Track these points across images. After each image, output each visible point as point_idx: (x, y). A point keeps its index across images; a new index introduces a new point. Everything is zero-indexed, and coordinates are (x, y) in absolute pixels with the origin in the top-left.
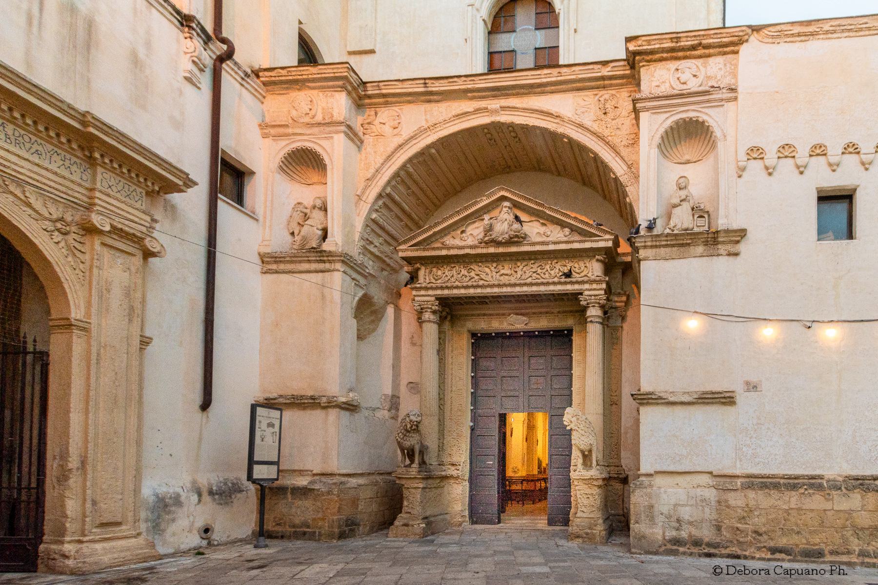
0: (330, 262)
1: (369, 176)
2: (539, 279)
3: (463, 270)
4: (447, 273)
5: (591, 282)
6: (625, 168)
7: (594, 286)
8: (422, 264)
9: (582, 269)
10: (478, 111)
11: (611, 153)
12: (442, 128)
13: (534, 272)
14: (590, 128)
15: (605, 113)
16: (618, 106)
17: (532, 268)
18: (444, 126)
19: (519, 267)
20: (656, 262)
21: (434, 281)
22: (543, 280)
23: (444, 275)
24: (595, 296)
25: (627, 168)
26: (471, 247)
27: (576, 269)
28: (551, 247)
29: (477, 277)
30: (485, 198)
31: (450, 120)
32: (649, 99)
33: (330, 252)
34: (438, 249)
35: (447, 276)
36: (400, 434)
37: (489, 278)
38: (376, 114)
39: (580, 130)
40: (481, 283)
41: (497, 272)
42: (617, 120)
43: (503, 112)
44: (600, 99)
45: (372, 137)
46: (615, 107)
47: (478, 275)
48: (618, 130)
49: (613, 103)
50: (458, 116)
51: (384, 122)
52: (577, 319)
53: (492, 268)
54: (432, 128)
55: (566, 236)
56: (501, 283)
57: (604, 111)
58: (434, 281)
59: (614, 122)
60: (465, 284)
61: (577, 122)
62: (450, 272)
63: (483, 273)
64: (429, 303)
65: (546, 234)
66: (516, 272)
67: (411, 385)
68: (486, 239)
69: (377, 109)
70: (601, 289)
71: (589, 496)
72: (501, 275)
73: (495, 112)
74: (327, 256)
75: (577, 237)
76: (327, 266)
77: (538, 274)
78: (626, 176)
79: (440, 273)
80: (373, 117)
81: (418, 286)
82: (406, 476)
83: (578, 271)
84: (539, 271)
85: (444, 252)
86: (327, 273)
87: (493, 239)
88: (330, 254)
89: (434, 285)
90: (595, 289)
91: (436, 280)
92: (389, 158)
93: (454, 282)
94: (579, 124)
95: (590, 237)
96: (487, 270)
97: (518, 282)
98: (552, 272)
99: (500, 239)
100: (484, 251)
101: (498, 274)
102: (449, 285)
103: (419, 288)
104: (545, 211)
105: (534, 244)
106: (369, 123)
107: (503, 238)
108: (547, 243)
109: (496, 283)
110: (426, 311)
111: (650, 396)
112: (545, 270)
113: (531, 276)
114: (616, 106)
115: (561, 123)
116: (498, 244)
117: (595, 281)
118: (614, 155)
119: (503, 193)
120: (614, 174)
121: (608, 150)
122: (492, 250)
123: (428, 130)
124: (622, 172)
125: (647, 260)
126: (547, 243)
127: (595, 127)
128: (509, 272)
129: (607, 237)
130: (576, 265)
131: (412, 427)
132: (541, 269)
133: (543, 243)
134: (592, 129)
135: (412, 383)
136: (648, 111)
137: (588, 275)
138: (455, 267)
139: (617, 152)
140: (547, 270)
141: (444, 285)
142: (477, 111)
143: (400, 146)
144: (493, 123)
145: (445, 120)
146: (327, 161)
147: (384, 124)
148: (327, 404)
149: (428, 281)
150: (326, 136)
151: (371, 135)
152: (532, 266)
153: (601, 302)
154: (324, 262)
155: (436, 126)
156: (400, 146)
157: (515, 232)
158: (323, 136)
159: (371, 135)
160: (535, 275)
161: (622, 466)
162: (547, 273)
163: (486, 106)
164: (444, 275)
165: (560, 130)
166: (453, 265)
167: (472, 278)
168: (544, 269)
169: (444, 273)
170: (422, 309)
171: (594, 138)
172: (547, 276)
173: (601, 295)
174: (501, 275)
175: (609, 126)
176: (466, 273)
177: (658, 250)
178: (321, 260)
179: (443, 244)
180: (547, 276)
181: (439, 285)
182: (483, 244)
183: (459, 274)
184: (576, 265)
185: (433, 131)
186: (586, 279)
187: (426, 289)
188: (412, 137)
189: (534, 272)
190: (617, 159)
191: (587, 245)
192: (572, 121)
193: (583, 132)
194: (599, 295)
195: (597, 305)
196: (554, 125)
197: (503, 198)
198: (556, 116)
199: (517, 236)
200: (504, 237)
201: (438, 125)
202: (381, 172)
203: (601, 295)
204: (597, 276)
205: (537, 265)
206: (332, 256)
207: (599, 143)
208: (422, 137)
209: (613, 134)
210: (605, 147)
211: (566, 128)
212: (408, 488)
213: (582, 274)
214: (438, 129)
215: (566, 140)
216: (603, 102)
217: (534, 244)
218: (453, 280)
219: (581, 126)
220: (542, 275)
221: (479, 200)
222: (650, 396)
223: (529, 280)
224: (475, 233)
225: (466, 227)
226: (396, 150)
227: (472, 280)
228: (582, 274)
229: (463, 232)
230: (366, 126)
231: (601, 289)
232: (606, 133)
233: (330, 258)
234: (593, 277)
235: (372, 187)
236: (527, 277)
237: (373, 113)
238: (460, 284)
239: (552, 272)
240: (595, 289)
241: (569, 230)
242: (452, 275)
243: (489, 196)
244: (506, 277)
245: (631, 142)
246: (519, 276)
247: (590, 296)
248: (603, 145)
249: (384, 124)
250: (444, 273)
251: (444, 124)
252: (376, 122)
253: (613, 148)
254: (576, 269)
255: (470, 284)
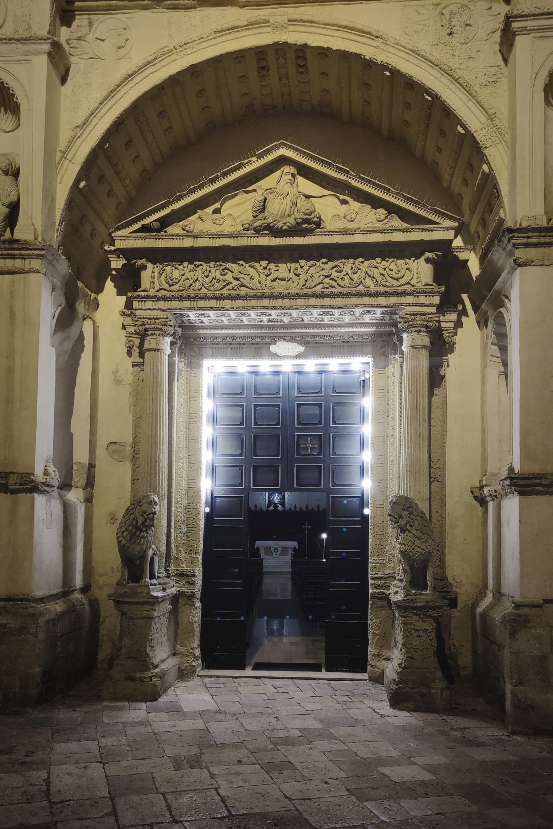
0: (23, 257)
1: (80, 121)
2: (334, 287)
3: (213, 270)
4: (187, 275)
5: (415, 293)
6: (484, 119)
7: (422, 299)
8: (149, 260)
9: (403, 272)
10: (252, 25)
11: (460, 95)
12: (194, 50)
13: (327, 277)
14: (430, 57)
15: (450, 34)
16: (471, 22)
17: (323, 269)
18: (199, 47)
19: (302, 267)
20: (544, 268)
21: (166, 286)
22: (342, 289)
23: (184, 278)
24: (421, 315)
25: (485, 119)
26: (231, 236)
27: (393, 273)
28: (358, 239)
29: (235, 283)
30: (254, 159)
31: (209, 38)
32: (534, 15)
33: (26, 242)
34: (178, 236)
35: (188, 279)
36: (126, 533)
37: (255, 284)
38: (90, 24)
39: (412, 59)
40: (243, 291)
41: (267, 276)
42: (470, 44)
43: (290, 28)
44: (444, 11)
45: (83, 61)
46: (467, 25)
47: (237, 279)
48: (471, 60)
49: (464, 18)
50: (222, 32)
51: (103, 38)
52: (378, 348)
53: (260, 269)
54: (180, 49)
55: (379, 221)
56: (276, 292)
57: (449, 31)
58: (166, 286)
59: (465, 46)
60: (218, 293)
61: (408, 46)
62: (192, 273)
63: (245, 277)
64: (158, 321)
65: (348, 218)
66: (298, 275)
67: (113, 447)
68: (257, 224)
69: (92, 16)
70: (431, 305)
71: (421, 633)
72: (274, 280)
73: (281, 27)
74: (20, 249)
75: (396, 222)
76: (18, 263)
77: (333, 279)
78: (484, 132)
79: (176, 274)
80: (85, 30)
81: (143, 294)
82: (132, 600)
83: (396, 276)
84: (334, 274)
85: (187, 243)
86: (18, 275)
87: (269, 224)
88: (25, 245)
89: (168, 294)
90: (422, 305)
91: (171, 285)
92: (112, 93)
93: (200, 290)
94: (411, 50)
95: (418, 224)
96: (252, 271)
97: (303, 292)
98: (355, 277)
99: (280, 225)
100: (252, 242)
101: (269, 278)
102: (193, 293)
103: (144, 297)
104: (350, 181)
105: (331, 233)
106: (79, 39)
107: (285, 224)
108: (352, 233)
109: (267, 291)
110: (152, 334)
111: (537, 481)
112: (344, 273)
113: (321, 283)
114: (468, 22)
115: (383, 46)
116: (275, 232)
117: (423, 293)
118: (465, 99)
119: (283, 151)
120: (464, 127)
121: (456, 91)
122: (265, 241)
123: (174, 51)
124: (479, 126)
125: (530, 265)
126: (352, 233)
127: (435, 54)
128: (286, 275)
129: (448, 223)
130: (393, 266)
131: (145, 521)
132: (336, 271)
133: (345, 232)
134: (433, 59)
135: (115, 443)
136: (529, 34)
137: (412, 282)
138: (201, 265)
139: (471, 95)
140: (347, 274)
141: (184, 294)
142: (252, 25)
143: (130, 76)
144: (276, 44)
145: (202, 38)
146: (20, 98)
147: (103, 40)
148: (18, 487)
149: (157, 286)
150: (20, 58)
151: (82, 57)
152: (323, 266)
153: (431, 324)
154: (13, 257)
155: (185, 47)
156: (130, 76)
157: (305, 214)
158: (15, 58)
159: (82, 57)
160: (327, 280)
161: (447, 580)
162: (347, 277)
163: (267, 18)
164: (184, 278)
165: (381, 57)
166: (197, 263)
167: (228, 284)
168: (341, 271)
169: (183, 275)
170: (146, 330)
171: (434, 72)
172: (347, 282)
173: (431, 314)
174: (274, 280)
175: (457, 53)
176: (218, 276)
177: (546, 250)
178: (8, 255)
179: (184, 229)
180: (347, 282)
181: (177, 294)
182: (251, 232)
183: (207, 277)
184: (393, 266)
185: (181, 54)
186: (408, 288)
187: (156, 298)
188: (149, 63)
189: (327, 277)
190: (470, 104)
191: (416, 236)
192: (401, 45)
193: (417, 62)
194: (428, 314)
195: (423, 329)
196: (371, 50)
197: (283, 161)
198: (377, 37)
199: (308, 221)
200: (285, 221)
201: (189, 45)
202: (98, 116)
203: (431, 314)
204: (427, 285)
205: (330, 264)
206: (28, 249)
207: (442, 79)
208: (163, 63)
209: (463, 66)
210: (452, 86)
211: (391, 55)
212: (133, 618)
213: (402, 281)
214: (188, 51)
215: (388, 74)
216: (448, 16)
217: (331, 233)
218: (197, 285)
219: (415, 53)
220: (339, 281)
221: (245, 161)
222: (537, 481)
223: (319, 289)
224: (236, 212)
225: (222, 205)
226: (123, 82)
227: (228, 287)
228: (402, 281)
229: (217, 211)
230: (74, 43)
231: (431, 305)
232: (453, 64)
233: (24, 252)
234: (419, 286)
235: (82, 138)
236: (315, 283)
237: (86, 22)
238: (209, 293)
239: (355, 277)
240: (422, 305)
241: (386, 212)
242: (196, 277)
243: (260, 157)
244: (283, 283)
245: (491, 80)
246: (302, 282)
247: (415, 315)
248: (449, 83)
249: (103, 40)
250: (183, 275)
251: (199, 43)
252: (90, 38)
253: (466, 88)
254: (393, 273)
255: (225, 292)
